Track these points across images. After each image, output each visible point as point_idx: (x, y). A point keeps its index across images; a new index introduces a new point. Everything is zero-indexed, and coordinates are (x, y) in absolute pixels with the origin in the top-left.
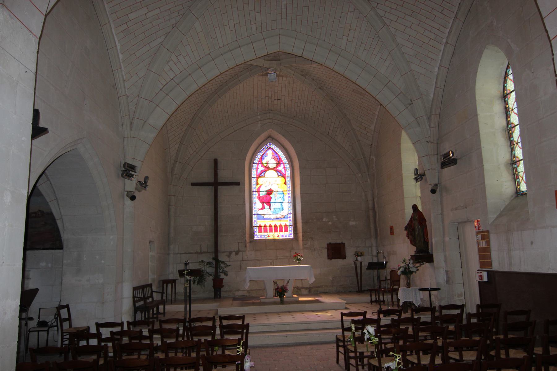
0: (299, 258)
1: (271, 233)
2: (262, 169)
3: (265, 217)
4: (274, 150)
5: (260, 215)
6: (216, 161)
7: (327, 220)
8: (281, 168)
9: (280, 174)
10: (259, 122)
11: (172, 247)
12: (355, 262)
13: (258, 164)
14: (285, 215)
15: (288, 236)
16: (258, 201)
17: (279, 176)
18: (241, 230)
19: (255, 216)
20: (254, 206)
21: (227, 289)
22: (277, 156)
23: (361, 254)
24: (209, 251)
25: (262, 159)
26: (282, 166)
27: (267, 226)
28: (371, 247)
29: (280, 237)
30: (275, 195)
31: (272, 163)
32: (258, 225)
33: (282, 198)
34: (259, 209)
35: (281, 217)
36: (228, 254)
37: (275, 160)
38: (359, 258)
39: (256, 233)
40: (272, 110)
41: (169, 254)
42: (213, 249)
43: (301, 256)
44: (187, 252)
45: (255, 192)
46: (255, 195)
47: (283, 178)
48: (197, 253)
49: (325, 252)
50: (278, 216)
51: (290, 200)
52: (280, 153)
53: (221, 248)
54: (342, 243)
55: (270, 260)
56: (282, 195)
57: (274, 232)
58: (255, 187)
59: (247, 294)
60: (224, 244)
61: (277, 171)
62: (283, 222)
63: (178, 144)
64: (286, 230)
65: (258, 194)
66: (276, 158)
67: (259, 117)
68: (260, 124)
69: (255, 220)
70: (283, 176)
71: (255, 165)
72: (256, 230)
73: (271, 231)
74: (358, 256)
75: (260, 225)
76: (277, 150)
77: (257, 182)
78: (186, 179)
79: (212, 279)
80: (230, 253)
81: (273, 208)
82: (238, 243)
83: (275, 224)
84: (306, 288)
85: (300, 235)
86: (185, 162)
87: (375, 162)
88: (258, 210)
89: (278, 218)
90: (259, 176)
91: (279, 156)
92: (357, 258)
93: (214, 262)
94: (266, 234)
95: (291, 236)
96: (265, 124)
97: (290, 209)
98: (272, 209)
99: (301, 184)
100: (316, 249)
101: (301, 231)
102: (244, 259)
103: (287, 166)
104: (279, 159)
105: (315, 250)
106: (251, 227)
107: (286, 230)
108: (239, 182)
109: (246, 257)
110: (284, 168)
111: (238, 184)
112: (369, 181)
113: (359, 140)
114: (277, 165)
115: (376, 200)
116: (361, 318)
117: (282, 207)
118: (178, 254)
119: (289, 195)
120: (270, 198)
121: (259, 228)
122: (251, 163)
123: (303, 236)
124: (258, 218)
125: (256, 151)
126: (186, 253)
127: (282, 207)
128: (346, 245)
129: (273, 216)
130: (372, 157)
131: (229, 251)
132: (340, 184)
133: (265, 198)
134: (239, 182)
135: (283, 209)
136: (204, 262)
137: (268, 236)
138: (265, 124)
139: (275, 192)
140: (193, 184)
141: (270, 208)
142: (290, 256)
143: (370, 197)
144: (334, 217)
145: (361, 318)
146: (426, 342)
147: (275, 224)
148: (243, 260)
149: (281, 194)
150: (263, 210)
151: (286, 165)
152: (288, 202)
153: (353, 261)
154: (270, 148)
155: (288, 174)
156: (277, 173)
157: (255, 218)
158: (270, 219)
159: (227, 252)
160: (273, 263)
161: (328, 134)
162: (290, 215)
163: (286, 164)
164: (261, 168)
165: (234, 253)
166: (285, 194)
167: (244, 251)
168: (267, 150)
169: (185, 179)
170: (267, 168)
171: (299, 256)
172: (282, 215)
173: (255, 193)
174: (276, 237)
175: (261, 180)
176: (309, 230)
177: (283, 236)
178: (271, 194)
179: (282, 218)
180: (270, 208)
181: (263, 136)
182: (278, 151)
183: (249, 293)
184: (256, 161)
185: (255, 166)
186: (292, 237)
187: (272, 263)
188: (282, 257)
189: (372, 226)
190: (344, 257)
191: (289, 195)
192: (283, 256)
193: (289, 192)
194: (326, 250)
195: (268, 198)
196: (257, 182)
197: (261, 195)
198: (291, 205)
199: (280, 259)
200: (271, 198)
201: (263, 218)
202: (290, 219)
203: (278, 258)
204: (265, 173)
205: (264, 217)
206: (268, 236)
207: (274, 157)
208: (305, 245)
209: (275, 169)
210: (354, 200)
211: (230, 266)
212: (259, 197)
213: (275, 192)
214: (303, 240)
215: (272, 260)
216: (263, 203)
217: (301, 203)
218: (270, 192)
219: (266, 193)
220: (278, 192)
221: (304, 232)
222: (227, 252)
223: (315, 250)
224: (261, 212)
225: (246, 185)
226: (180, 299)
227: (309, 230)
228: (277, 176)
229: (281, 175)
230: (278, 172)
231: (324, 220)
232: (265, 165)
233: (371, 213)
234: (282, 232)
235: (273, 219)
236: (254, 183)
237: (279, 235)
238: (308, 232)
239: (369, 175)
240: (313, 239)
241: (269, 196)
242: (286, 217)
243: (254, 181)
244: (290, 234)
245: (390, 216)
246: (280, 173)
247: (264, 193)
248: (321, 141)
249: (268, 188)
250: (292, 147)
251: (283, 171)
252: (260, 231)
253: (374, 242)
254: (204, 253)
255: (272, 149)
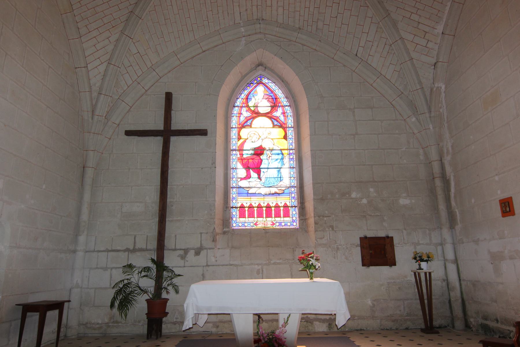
0: (310, 263)
1: (260, 219)
2: (248, 114)
3: (251, 191)
4: (267, 87)
5: (243, 188)
6: (169, 97)
7: (358, 196)
8: (278, 113)
9: (276, 123)
10: (244, 38)
11: (82, 239)
12: (415, 273)
13: (242, 107)
14: (284, 189)
16: (239, 166)
17: (274, 126)
18: (206, 212)
19: (234, 190)
20: (233, 173)
21: (176, 318)
22: (272, 95)
23: (429, 257)
24: (149, 248)
25: (247, 98)
26: (280, 110)
27: (254, 207)
28: (442, 244)
29: (277, 226)
30: (268, 156)
31: (264, 106)
32: (239, 205)
34: (242, 179)
35: (278, 191)
36: (182, 252)
37: (268, 101)
38: (424, 265)
39: (234, 219)
40: (263, 19)
41: (74, 251)
42: (153, 245)
43: (314, 258)
44: (110, 249)
45: (235, 150)
46: (235, 156)
47: (281, 130)
48: (127, 250)
49: (357, 253)
50: (273, 190)
51: (293, 163)
53: (169, 243)
54: (388, 237)
55: (256, 266)
56: (280, 156)
57: (266, 217)
58: (235, 144)
59: (214, 330)
60: (176, 236)
61: (271, 118)
62: (281, 201)
63: (105, 64)
64: (286, 215)
65: (240, 154)
66: (271, 97)
67: (243, 29)
68: (244, 42)
69: (234, 196)
70: (281, 126)
71: (237, 108)
72: (235, 213)
73: (260, 215)
74: (422, 260)
75: (242, 204)
76: (272, 86)
77: (239, 135)
78: (119, 125)
79: (146, 300)
80: (186, 251)
81: (264, 176)
82: (201, 233)
83: (268, 204)
84: (323, 321)
85: (311, 221)
86: (117, 98)
87: (445, 92)
88: (239, 180)
89: (273, 194)
90: (243, 126)
91: (275, 95)
92: (420, 265)
93: (154, 267)
94: (251, 219)
95: (295, 224)
96: (252, 41)
97: (292, 178)
98: (262, 179)
99: (311, 135)
100: (340, 247)
101: (313, 215)
102: (209, 264)
103: (288, 110)
104: (274, 99)
105: (338, 249)
106: (227, 206)
107: (286, 215)
108: (206, 130)
109: (213, 259)
110: (284, 113)
111: (203, 133)
112: (431, 128)
113: (412, 59)
114: (271, 110)
115: (447, 159)
118: (94, 251)
119: (291, 157)
120: (260, 160)
121: (239, 211)
122: (230, 105)
123: (316, 223)
124: (239, 194)
125: (238, 86)
126: (108, 251)
128: (395, 241)
129: (264, 191)
130: (436, 85)
131: (183, 248)
132: (379, 134)
133: (250, 161)
134: (206, 130)
135: (281, 179)
136: (135, 267)
137: (256, 224)
138: (252, 41)
139: (268, 152)
140: (129, 133)
141: (259, 178)
142: (294, 259)
143: (434, 155)
144: (372, 190)
146: (232, 228)
147: (268, 204)
148: (207, 266)
149: (278, 154)
150: (249, 180)
152: (290, 168)
153: (412, 271)
154: (260, 83)
155: (290, 122)
156: (272, 122)
157: (233, 193)
158: (260, 194)
159: (181, 249)
160: (263, 271)
161: (356, 55)
162: (293, 189)
163: (287, 107)
164: (246, 114)
165: (192, 252)
166: (285, 155)
167: (210, 249)
168: (255, 87)
169: (116, 125)
170: (256, 114)
171: (311, 258)
172: (278, 188)
173: (234, 152)
174: (269, 225)
175: (244, 133)
176: (327, 212)
177: (280, 224)
178: (262, 154)
179: (279, 194)
180: (259, 178)
181: (251, 59)
183: (218, 327)
184: (239, 103)
185: (236, 110)
186: (296, 225)
187: (261, 272)
188: (278, 261)
189: (442, 207)
190: (392, 263)
192: (280, 259)
193: (291, 152)
194: (359, 249)
195: (257, 162)
196: (239, 135)
197: (245, 156)
198: (294, 173)
199: (275, 263)
200: (262, 160)
201: (248, 193)
203: (272, 262)
204: (252, 122)
205: (249, 192)
206: (256, 224)
207: (267, 97)
208: (321, 238)
209: (269, 115)
210: (405, 161)
211: (179, 275)
212: (241, 159)
213: (267, 150)
214: (316, 231)
215: (260, 266)
216: (247, 167)
217: (312, 166)
218: (259, 152)
219: (253, 152)
220: (274, 152)
221: (318, 216)
222: (181, 249)
223: (338, 249)
224: (244, 183)
225: (218, 136)
226: (90, 335)
227: (327, 212)
228: (272, 126)
229: (279, 124)
230: (273, 120)
231: (354, 195)
232: (253, 109)
233: (438, 183)
234: (280, 216)
235: (264, 195)
237: (274, 222)
238: (326, 217)
239: (430, 117)
240: (335, 229)
241: (258, 158)
242: (286, 191)
243: (234, 133)
244: (294, 221)
245: (497, 178)
246: (277, 121)
247: (250, 153)
248: (344, 66)
249: (257, 145)
250: (297, 77)
251: (282, 118)
252: (242, 215)
253: (446, 234)
254: (141, 250)
255: (264, 84)
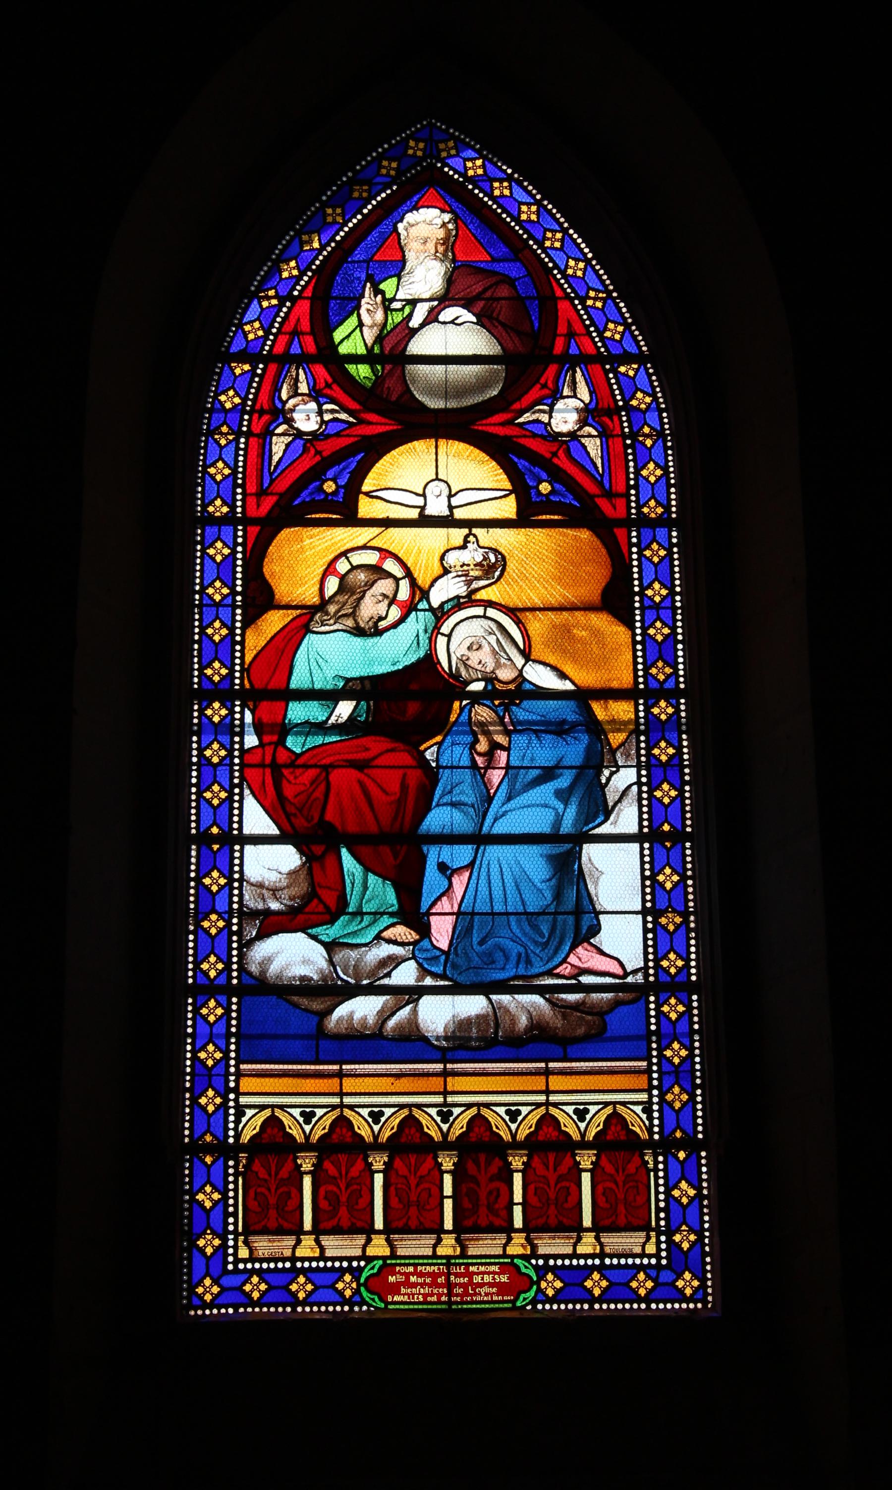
15: (643, 1284)
19: (212, 1010)
22: (514, 270)
33: (564, 781)
52: (554, 240)
66: (504, 291)
69: (210, 1055)
95: (687, 1282)
116: (510, 1305)
117: (571, 895)
119: (664, 752)
127: (571, 895)
133: (342, 778)
145: (510, 1305)
151: (630, 388)
162: (673, 1009)
182: (528, 213)
191: (664, 752)
193: (663, 710)
195: (395, 787)
201: (321, 1033)
202: (676, 1052)
209: (492, 425)
220: (526, 711)
229: (569, 499)
230: (522, 464)
236: (217, 592)
242: (617, 1023)
